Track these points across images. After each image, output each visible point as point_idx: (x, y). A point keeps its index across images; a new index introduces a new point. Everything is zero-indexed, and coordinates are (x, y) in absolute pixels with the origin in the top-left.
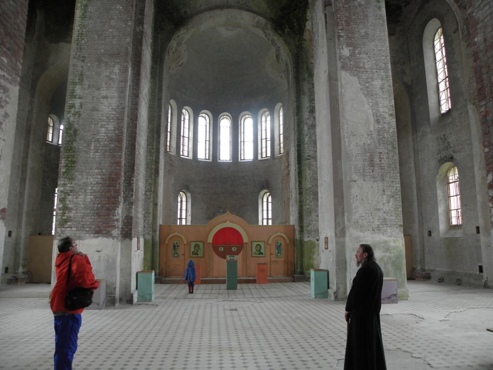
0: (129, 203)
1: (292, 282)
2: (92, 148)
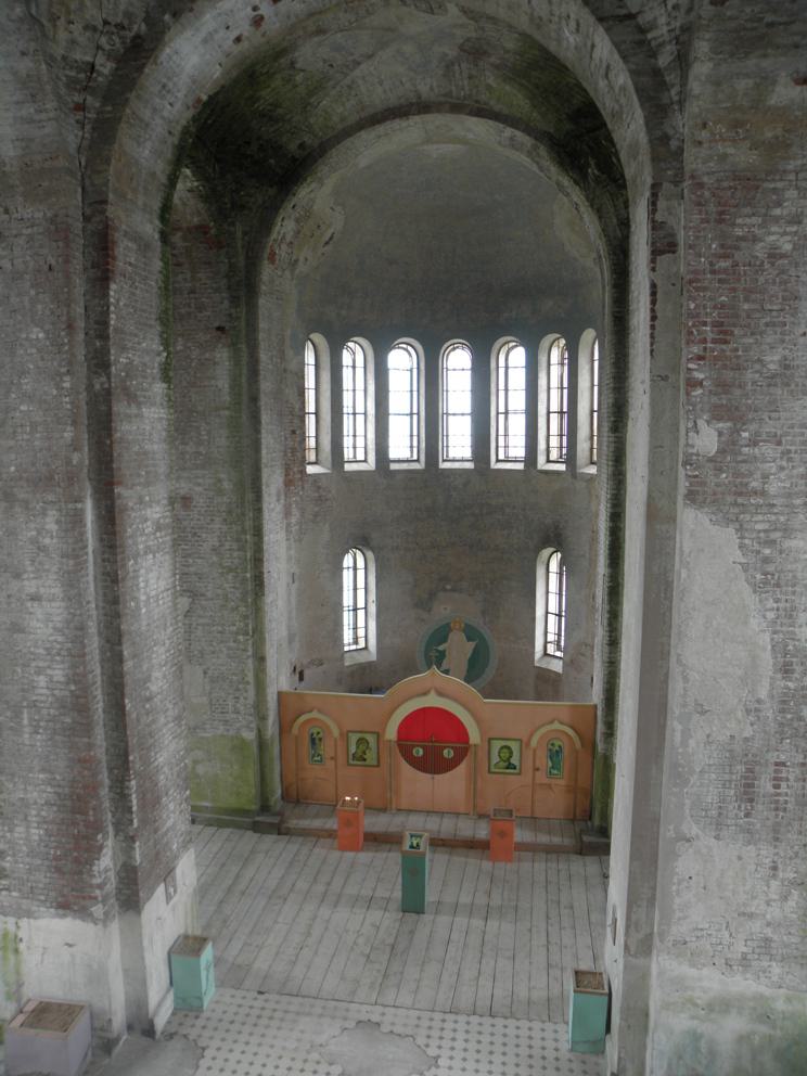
0: (126, 837)
1: (577, 853)
2: (26, 722)
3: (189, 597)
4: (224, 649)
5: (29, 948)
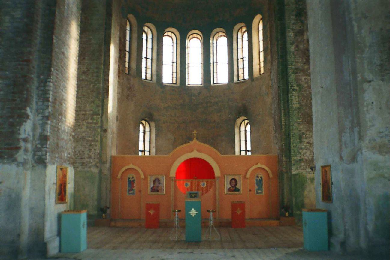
4: (85, 123)
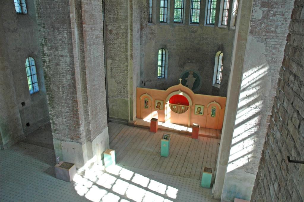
3: (112, 60)
5: (64, 148)
